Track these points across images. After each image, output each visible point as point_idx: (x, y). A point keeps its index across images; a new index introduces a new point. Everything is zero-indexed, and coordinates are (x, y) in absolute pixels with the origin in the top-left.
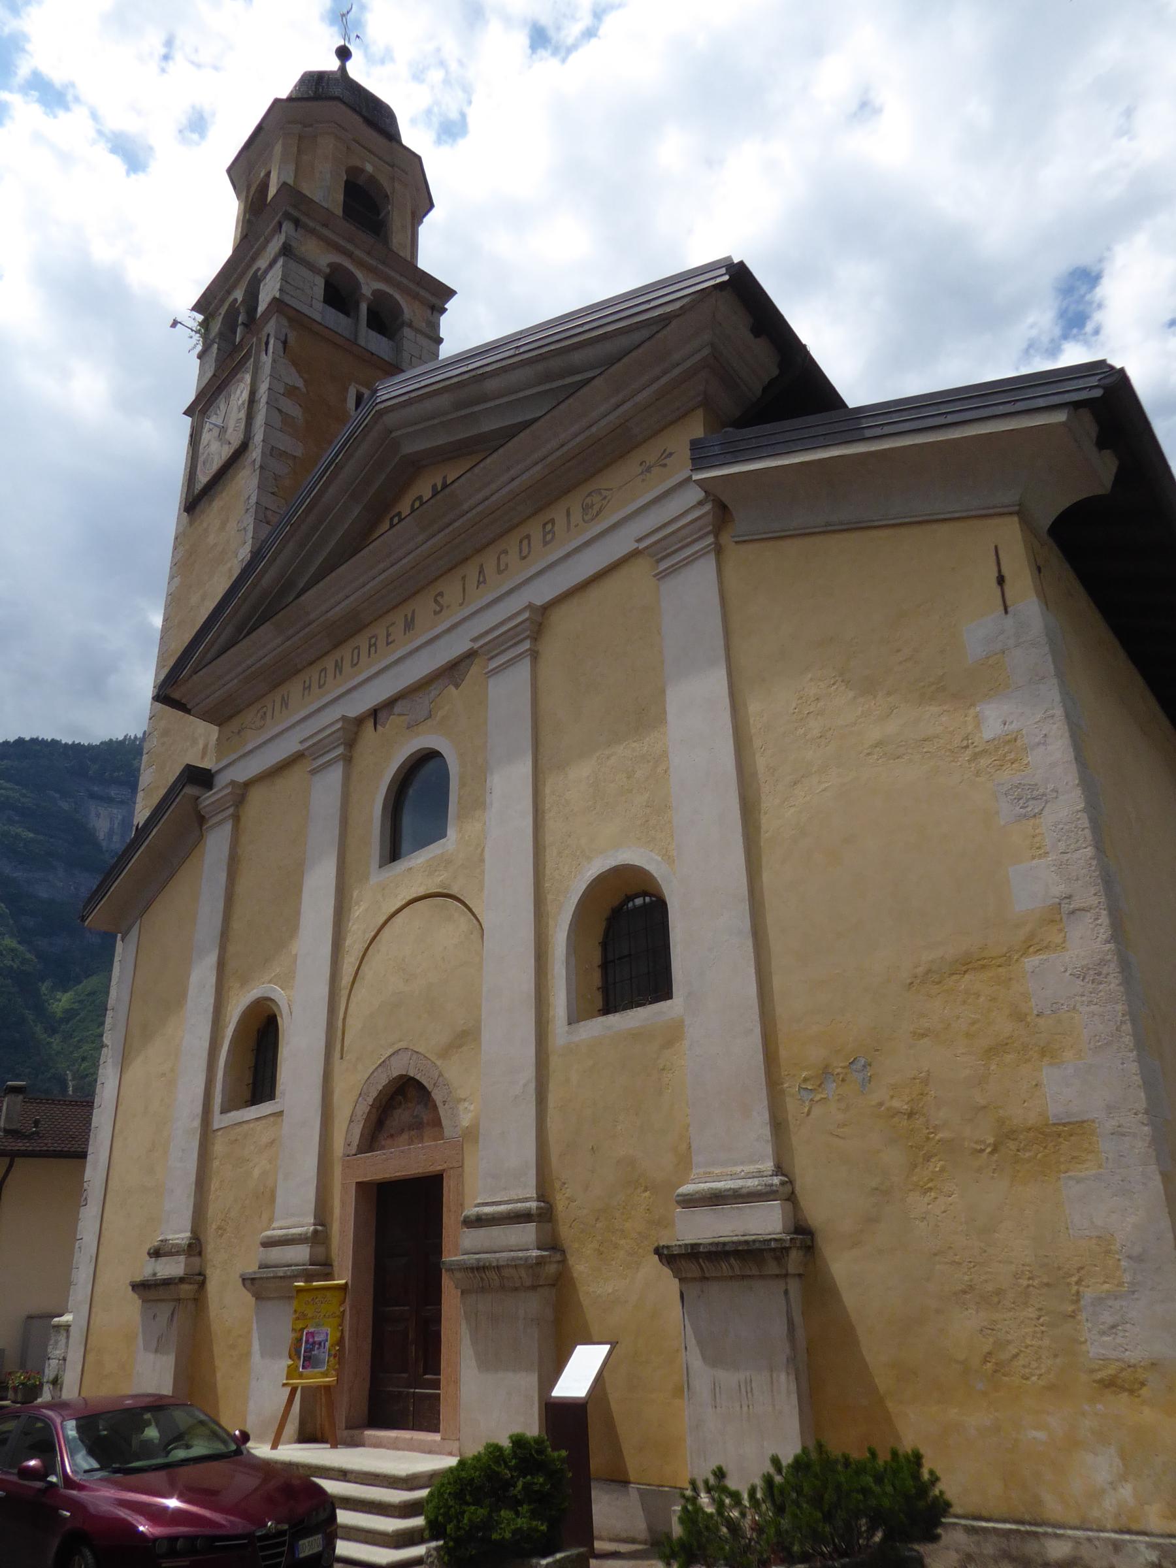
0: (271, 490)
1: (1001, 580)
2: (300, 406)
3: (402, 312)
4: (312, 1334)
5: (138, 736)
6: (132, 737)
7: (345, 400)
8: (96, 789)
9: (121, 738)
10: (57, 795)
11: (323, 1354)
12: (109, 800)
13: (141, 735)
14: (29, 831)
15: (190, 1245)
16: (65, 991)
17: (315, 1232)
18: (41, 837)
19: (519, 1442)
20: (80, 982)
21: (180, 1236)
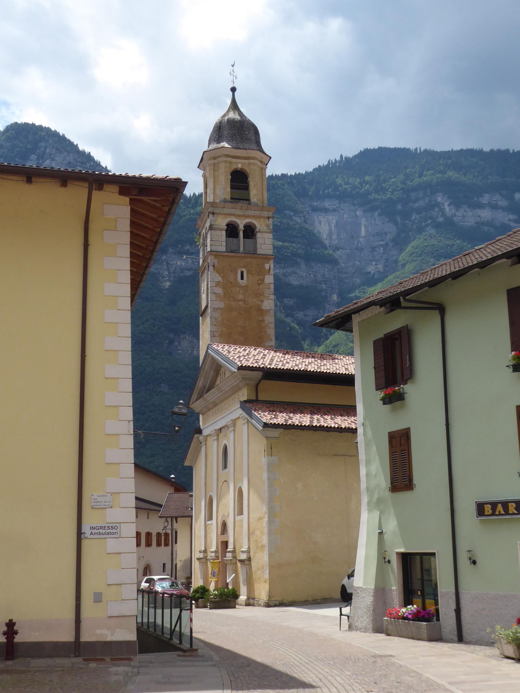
0: (215, 324)
1: (271, 448)
2: (221, 288)
3: (256, 227)
4: (214, 571)
5: (338, 160)
6: (333, 161)
7: (237, 277)
8: (315, 204)
9: (326, 163)
10: (292, 213)
11: (216, 574)
12: (326, 210)
13: (339, 159)
14: (279, 241)
15: (204, 551)
16: (319, 346)
17: (216, 550)
18: (286, 244)
19: (201, 586)
20: (328, 339)
21: (203, 549)
